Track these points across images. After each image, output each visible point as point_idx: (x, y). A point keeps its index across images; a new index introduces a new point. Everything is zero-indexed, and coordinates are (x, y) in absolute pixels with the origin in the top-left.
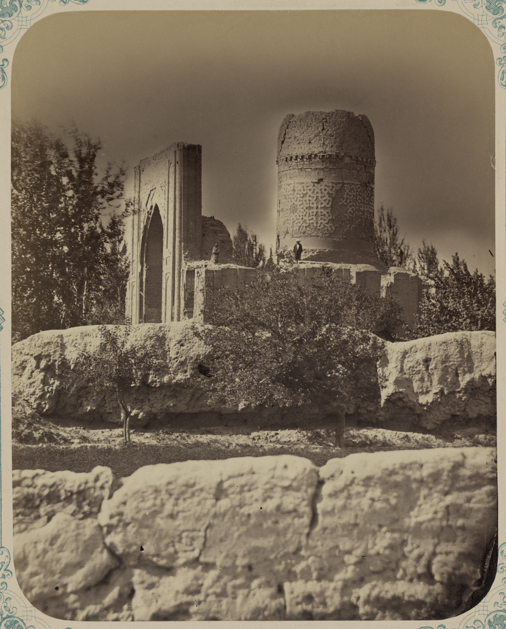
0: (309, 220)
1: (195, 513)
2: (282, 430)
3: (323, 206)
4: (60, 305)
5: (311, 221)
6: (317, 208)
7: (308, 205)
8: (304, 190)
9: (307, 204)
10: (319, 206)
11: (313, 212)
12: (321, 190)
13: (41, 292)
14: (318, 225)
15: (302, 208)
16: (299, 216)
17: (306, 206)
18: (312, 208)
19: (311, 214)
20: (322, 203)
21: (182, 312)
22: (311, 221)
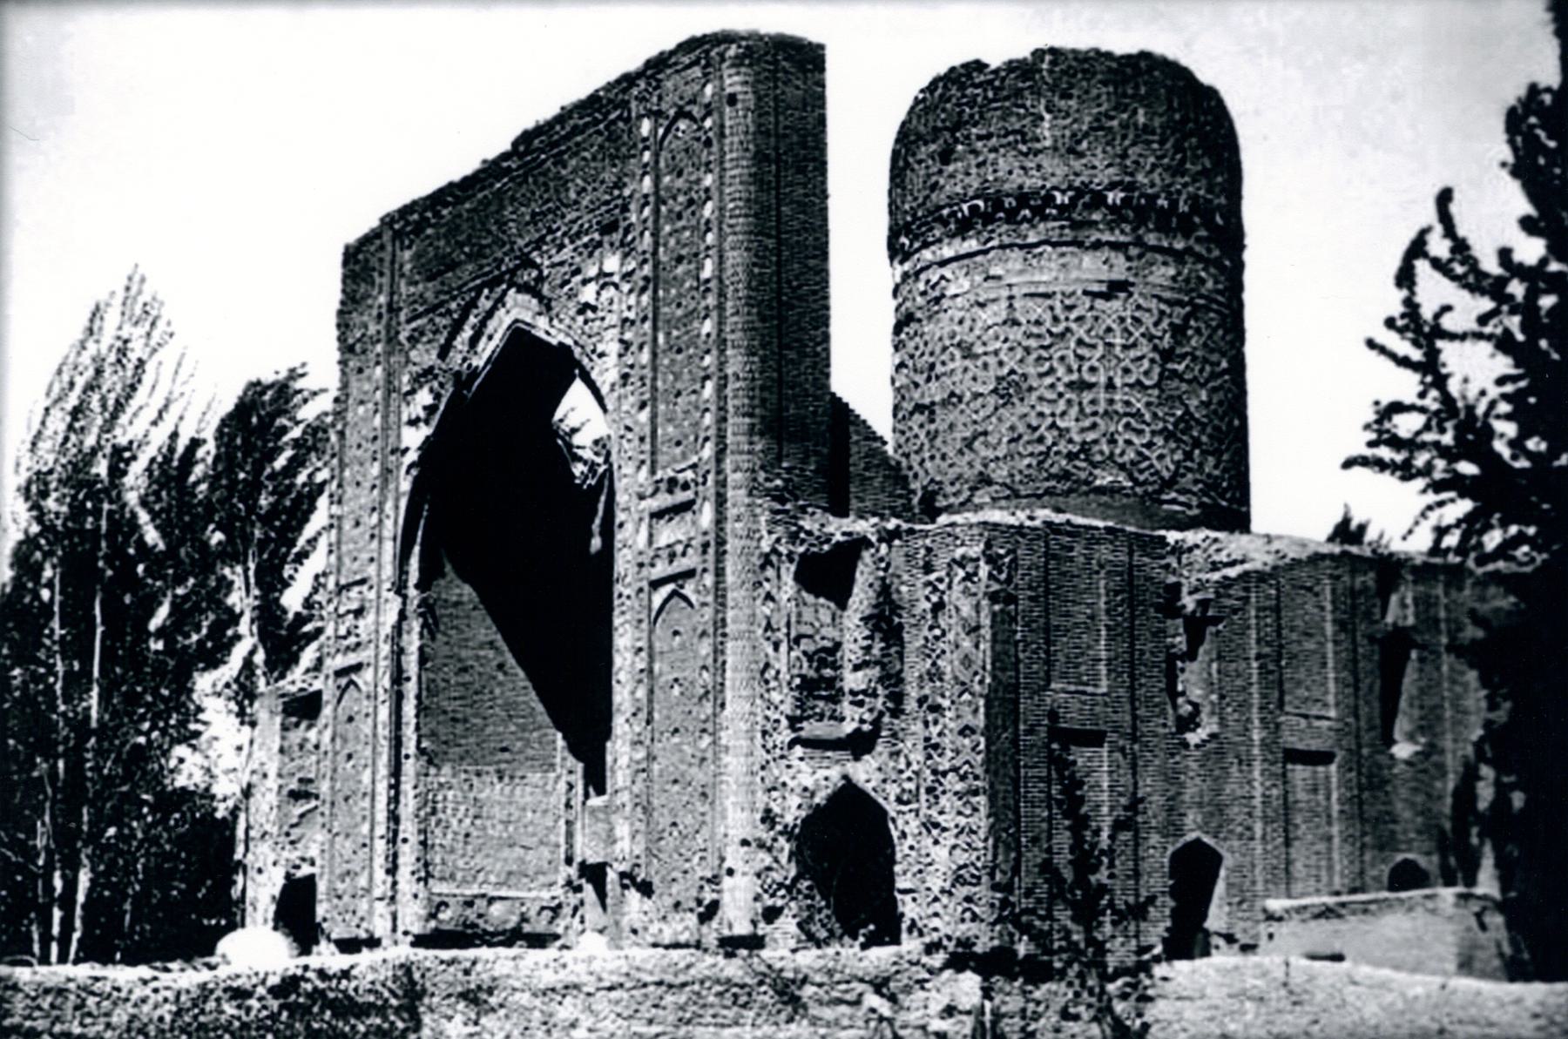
0: (1083, 430)
1: (1021, 187)
2: (428, 438)
3: (1131, 379)
4: (47, 609)
5: (1090, 436)
6: (1110, 386)
7: (1075, 377)
8: (1056, 319)
9: (1070, 370)
10: (1118, 382)
11: (1093, 402)
12: (1122, 320)
13: (100, 926)
14: (1118, 451)
15: (1052, 386)
16: (1041, 414)
17: (1066, 379)
18: (1091, 386)
19: (1088, 410)
20: (1126, 371)
21: (410, 747)
22: (1090, 436)
